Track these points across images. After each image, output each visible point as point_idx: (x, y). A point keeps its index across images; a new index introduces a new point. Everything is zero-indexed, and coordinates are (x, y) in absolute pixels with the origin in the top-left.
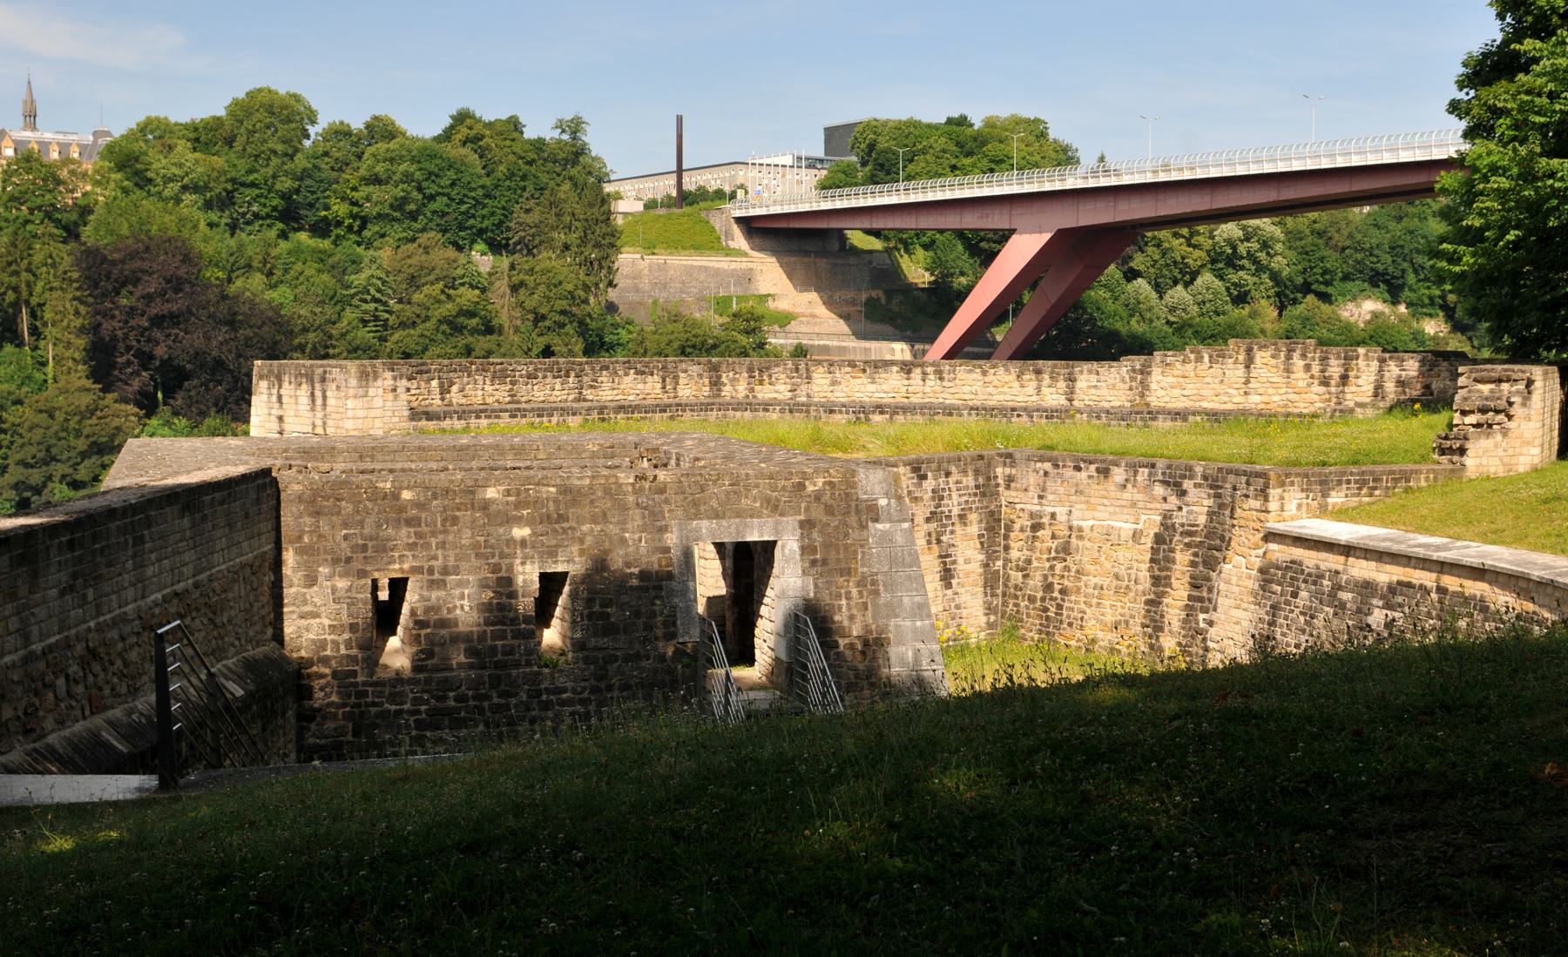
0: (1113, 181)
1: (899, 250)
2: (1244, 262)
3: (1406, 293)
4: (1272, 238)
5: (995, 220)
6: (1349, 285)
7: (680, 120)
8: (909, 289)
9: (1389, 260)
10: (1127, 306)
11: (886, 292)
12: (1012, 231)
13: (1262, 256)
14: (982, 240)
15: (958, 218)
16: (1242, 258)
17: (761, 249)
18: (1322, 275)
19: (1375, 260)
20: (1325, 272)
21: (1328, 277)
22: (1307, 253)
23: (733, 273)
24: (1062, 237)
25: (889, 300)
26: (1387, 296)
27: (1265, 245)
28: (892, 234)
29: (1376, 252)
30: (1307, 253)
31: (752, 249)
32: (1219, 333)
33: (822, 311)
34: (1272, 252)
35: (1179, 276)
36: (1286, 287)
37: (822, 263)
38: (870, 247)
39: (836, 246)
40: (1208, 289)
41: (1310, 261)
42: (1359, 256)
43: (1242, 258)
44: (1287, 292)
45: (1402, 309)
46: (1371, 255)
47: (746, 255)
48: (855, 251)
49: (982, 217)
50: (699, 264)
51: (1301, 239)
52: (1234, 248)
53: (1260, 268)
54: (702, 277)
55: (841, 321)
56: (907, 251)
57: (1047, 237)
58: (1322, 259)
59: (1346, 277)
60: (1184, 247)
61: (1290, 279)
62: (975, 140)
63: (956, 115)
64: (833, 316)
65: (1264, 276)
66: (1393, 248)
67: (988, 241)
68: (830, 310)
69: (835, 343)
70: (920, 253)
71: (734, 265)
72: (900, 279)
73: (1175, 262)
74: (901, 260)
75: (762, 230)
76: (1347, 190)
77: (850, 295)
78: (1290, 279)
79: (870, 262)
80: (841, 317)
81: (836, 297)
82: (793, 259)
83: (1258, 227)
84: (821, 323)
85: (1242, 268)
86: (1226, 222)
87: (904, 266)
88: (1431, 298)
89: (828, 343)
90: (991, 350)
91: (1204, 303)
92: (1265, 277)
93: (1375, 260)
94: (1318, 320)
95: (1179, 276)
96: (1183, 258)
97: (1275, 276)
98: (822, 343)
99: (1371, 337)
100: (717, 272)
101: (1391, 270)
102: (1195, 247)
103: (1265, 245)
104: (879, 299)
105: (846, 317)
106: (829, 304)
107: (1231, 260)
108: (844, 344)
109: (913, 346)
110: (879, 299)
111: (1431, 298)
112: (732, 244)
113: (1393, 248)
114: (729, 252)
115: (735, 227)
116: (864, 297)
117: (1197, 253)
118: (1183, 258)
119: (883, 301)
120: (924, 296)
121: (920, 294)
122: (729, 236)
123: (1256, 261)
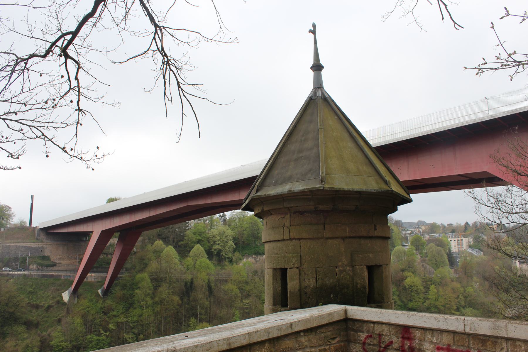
69: (56, 274)
90: (106, 275)
98: (51, 273)
108: (60, 274)
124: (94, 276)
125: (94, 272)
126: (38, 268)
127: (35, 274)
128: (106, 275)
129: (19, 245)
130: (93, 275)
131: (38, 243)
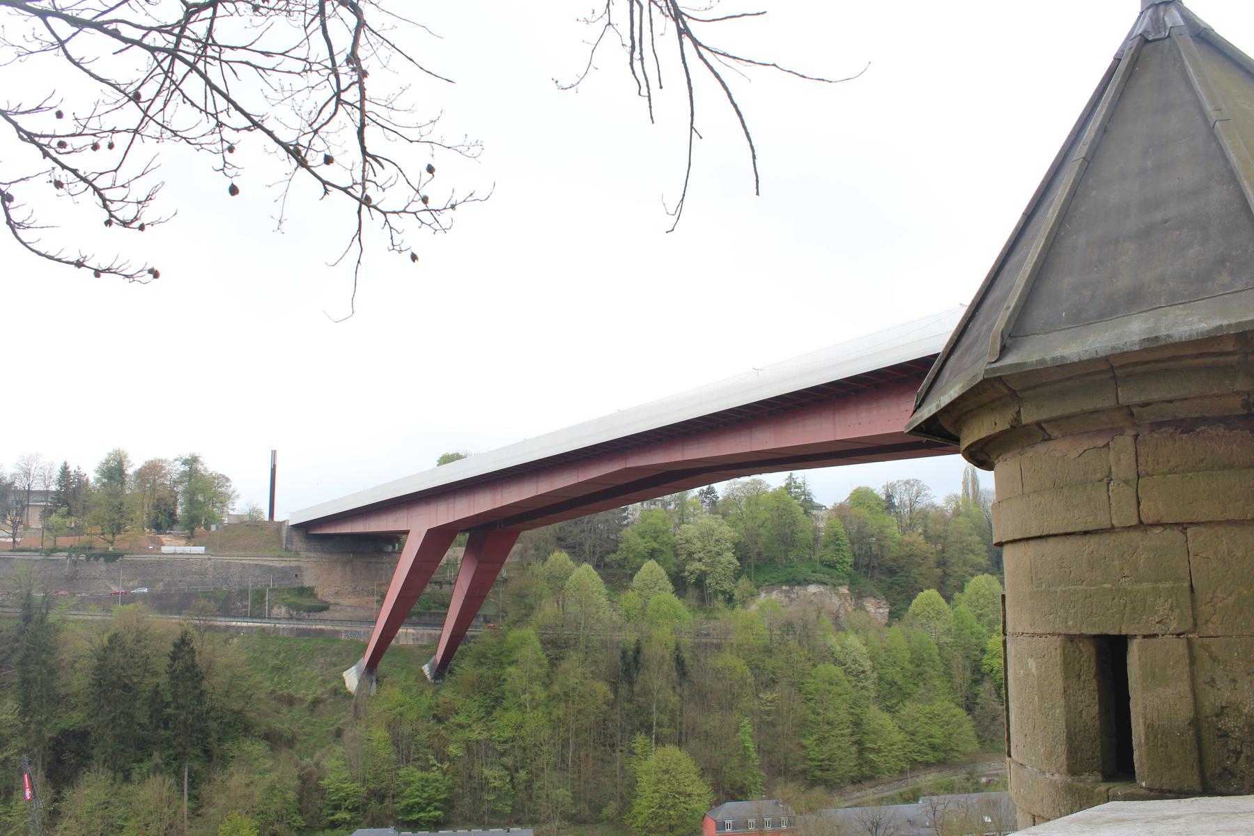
7: (274, 453)
69: (330, 627)
89: (323, 627)
90: (438, 632)
98: (318, 627)
124: (413, 634)
125: (414, 625)
126: (291, 615)
127: (284, 628)
128: (438, 632)
129: (247, 562)
130: (410, 631)
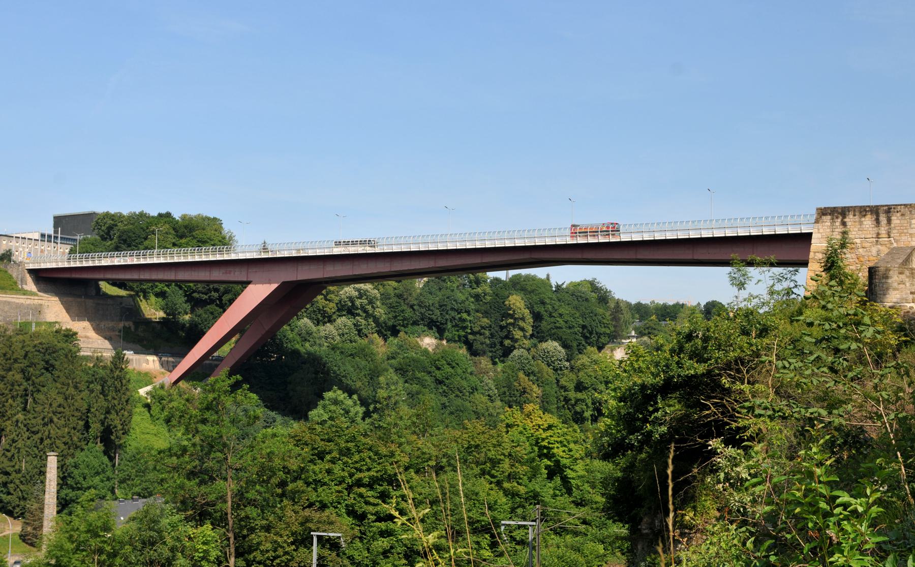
0: (270, 255)
1: (139, 297)
2: (359, 311)
3: (446, 334)
4: (375, 297)
5: (237, 275)
6: (416, 328)
8: (148, 322)
9: (439, 314)
10: (300, 335)
11: (135, 323)
12: (249, 283)
13: (369, 307)
14: (194, 292)
15: (207, 274)
16: (357, 309)
17: (45, 292)
18: (403, 320)
19: (431, 313)
20: (404, 319)
21: (405, 322)
22: (393, 307)
23: (28, 307)
24: (284, 286)
25: (136, 328)
26: (437, 335)
27: (371, 302)
28: (135, 285)
29: (432, 308)
30: (393, 307)
31: (39, 291)
32: (356, 353)
33: (92, 334)
34: (375, 306)
35: (321, 318)
36: (383, 327)
37: (90, 303)
38: (115, 294)
39: (94, 293)
40: (345, 326)
41: (395, 312)
42: (423, 310)
43: (357, 309)
44: (383, 330)
45: (444, 342)
46: (429, 310)
47: (37, 295)
48: (106, 296)
49: (226, 273)
50: (4, 299)
51: (390, 299)
52: (352, 301)
53: (368, 315)
54: (6, 309)
55: (107, 342)
56: (145, 297)
57: (274, 286)
58: (403, 311)
59: (415, 323)
60: (324, 301)
61: (385, 323)
62: (186, 227)
63: (164, 211)
64: (100, 337)
65: (370, 320)
66: (441, 306)
67: (199, 292)
68: (97, 334)
70: (153, 298)
71: (28, 302)
72: (140, 315)
73: (319, 310)
74: (140, 303)
75: (45, 278)
76: (479, 261)
77: (111, 324)
78: (385, 323)
79: (121, 303)
80: (105, 338)
81: (102, 325)
82: (70, 299)
83: (367, 290)
84: (93, 342)
85: (358, 315)
86: (348, 285)
87: (142, 307)
88: (459, 336)
91: (343, 335)
92: (370, 320)
93: (431, 313)
94: (408, 347)
95: (321, 318)
96: (323, 307)
97: (376, 320)
99: (442, 357)
100: (19, 306)
101: (439, 319)
102: (329, 301)
103: (371, 302)
104: (130, 328)
105: (109, 339)
106: (97, 330)
107: (351, 310)
109: (161, 358)
110: (130, 328)
111: (459, 336)
112: (25, 287)
113: (441, 306)
114: (25, 293)
115: (28, 275)
116: (121, 325)
117: (332, 305)
118: (323, 307)
119: (133, 329)
120: (158, 327)
121: (156, 325)
122: (23, 281)
123: (365, 311)
124: (173, 362)
131: (32, 297)
